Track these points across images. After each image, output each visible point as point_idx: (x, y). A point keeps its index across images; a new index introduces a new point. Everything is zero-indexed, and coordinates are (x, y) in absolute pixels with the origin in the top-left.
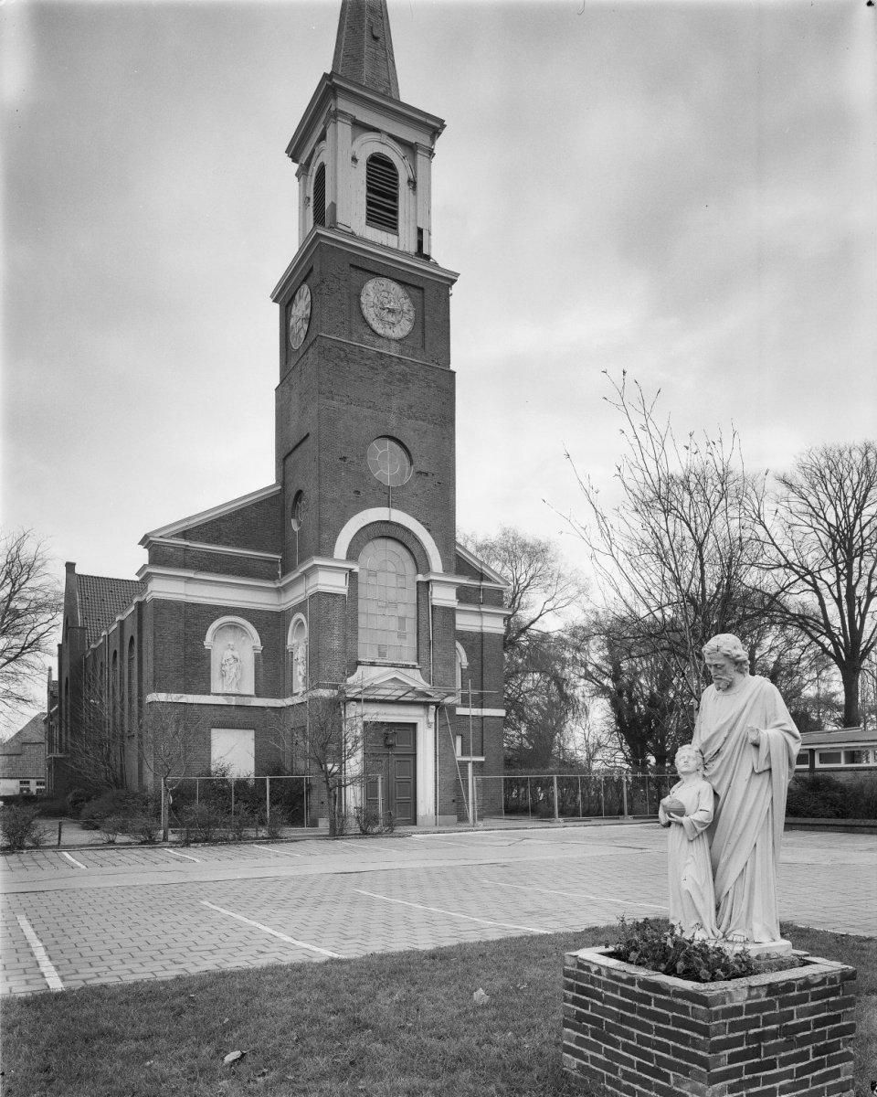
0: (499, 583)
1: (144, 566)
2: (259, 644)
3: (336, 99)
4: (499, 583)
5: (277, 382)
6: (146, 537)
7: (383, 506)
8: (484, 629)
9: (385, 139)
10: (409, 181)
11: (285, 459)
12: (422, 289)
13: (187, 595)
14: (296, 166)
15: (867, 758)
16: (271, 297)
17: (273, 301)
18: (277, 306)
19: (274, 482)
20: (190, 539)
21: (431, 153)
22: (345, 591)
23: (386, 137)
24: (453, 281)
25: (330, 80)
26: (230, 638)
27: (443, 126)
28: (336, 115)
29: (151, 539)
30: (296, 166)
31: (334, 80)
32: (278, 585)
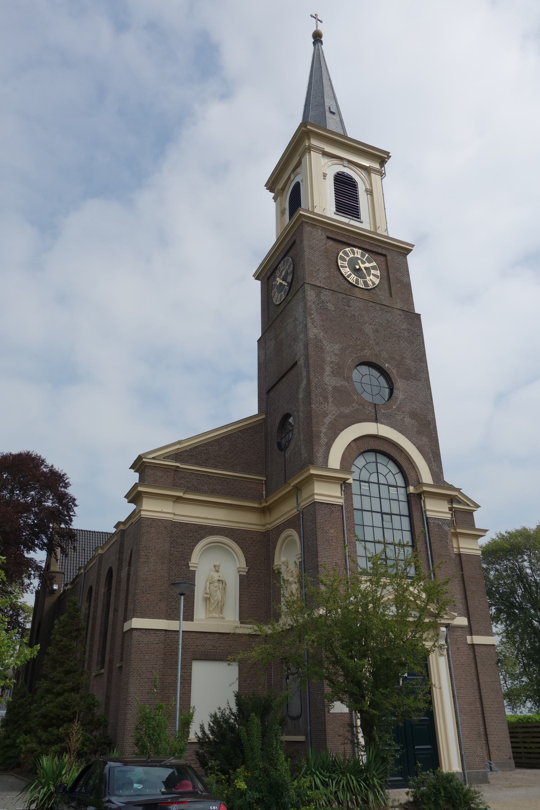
0: (468, 505)
1: (136, 486)
2: (244, 565)
3: (309, 139)
4: (468, 505)
5: (259, 335)
6: (140, 458)
7: (372, 421)
8: (461, 550)
9: (346, 163)
10: (366, 190)
11: (268, 392)
12: (385, 256)
13: (174, 514)
14: (273, 195)
15: (113, 751)
16: (254, 276)
17: (255, 279)
18: (259, 283)
19: (256, 412)
20: (181, 461)
21: (382, 175)
22: (341, 501)
23: (347, 162)
24: (409, 251)
25: (306, 127)
26: (216, 558)
27: (389, 157)
28: (309, 149)
29: (144, 460)
30: (273, 195)
31: (308, 127)
32: (264, 504)
